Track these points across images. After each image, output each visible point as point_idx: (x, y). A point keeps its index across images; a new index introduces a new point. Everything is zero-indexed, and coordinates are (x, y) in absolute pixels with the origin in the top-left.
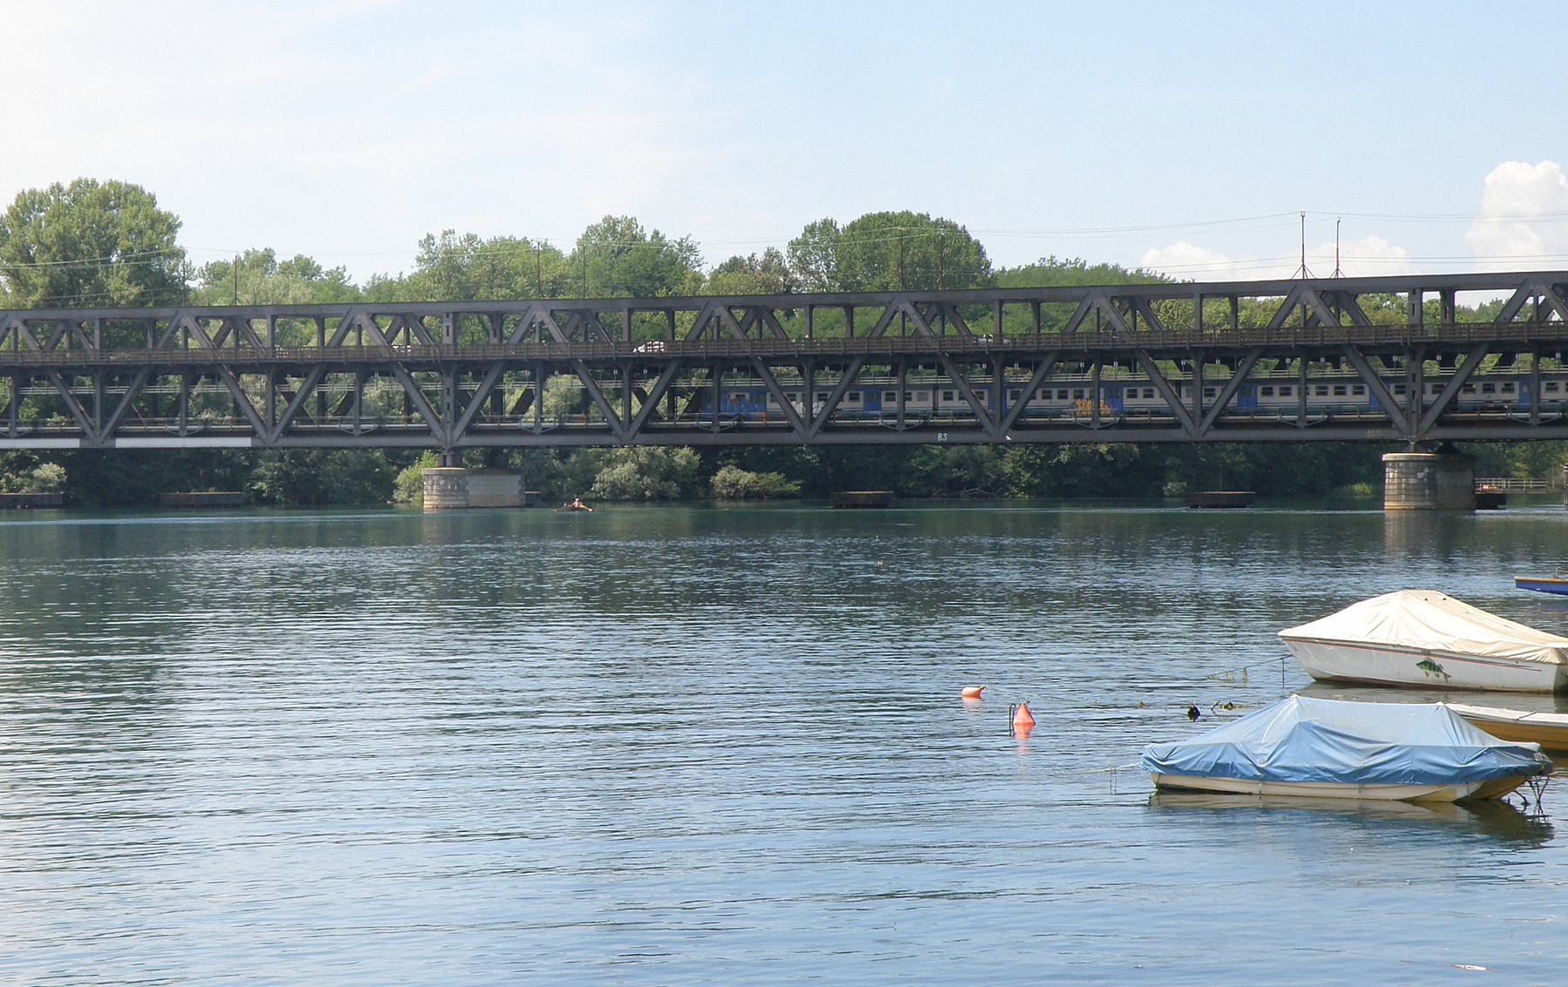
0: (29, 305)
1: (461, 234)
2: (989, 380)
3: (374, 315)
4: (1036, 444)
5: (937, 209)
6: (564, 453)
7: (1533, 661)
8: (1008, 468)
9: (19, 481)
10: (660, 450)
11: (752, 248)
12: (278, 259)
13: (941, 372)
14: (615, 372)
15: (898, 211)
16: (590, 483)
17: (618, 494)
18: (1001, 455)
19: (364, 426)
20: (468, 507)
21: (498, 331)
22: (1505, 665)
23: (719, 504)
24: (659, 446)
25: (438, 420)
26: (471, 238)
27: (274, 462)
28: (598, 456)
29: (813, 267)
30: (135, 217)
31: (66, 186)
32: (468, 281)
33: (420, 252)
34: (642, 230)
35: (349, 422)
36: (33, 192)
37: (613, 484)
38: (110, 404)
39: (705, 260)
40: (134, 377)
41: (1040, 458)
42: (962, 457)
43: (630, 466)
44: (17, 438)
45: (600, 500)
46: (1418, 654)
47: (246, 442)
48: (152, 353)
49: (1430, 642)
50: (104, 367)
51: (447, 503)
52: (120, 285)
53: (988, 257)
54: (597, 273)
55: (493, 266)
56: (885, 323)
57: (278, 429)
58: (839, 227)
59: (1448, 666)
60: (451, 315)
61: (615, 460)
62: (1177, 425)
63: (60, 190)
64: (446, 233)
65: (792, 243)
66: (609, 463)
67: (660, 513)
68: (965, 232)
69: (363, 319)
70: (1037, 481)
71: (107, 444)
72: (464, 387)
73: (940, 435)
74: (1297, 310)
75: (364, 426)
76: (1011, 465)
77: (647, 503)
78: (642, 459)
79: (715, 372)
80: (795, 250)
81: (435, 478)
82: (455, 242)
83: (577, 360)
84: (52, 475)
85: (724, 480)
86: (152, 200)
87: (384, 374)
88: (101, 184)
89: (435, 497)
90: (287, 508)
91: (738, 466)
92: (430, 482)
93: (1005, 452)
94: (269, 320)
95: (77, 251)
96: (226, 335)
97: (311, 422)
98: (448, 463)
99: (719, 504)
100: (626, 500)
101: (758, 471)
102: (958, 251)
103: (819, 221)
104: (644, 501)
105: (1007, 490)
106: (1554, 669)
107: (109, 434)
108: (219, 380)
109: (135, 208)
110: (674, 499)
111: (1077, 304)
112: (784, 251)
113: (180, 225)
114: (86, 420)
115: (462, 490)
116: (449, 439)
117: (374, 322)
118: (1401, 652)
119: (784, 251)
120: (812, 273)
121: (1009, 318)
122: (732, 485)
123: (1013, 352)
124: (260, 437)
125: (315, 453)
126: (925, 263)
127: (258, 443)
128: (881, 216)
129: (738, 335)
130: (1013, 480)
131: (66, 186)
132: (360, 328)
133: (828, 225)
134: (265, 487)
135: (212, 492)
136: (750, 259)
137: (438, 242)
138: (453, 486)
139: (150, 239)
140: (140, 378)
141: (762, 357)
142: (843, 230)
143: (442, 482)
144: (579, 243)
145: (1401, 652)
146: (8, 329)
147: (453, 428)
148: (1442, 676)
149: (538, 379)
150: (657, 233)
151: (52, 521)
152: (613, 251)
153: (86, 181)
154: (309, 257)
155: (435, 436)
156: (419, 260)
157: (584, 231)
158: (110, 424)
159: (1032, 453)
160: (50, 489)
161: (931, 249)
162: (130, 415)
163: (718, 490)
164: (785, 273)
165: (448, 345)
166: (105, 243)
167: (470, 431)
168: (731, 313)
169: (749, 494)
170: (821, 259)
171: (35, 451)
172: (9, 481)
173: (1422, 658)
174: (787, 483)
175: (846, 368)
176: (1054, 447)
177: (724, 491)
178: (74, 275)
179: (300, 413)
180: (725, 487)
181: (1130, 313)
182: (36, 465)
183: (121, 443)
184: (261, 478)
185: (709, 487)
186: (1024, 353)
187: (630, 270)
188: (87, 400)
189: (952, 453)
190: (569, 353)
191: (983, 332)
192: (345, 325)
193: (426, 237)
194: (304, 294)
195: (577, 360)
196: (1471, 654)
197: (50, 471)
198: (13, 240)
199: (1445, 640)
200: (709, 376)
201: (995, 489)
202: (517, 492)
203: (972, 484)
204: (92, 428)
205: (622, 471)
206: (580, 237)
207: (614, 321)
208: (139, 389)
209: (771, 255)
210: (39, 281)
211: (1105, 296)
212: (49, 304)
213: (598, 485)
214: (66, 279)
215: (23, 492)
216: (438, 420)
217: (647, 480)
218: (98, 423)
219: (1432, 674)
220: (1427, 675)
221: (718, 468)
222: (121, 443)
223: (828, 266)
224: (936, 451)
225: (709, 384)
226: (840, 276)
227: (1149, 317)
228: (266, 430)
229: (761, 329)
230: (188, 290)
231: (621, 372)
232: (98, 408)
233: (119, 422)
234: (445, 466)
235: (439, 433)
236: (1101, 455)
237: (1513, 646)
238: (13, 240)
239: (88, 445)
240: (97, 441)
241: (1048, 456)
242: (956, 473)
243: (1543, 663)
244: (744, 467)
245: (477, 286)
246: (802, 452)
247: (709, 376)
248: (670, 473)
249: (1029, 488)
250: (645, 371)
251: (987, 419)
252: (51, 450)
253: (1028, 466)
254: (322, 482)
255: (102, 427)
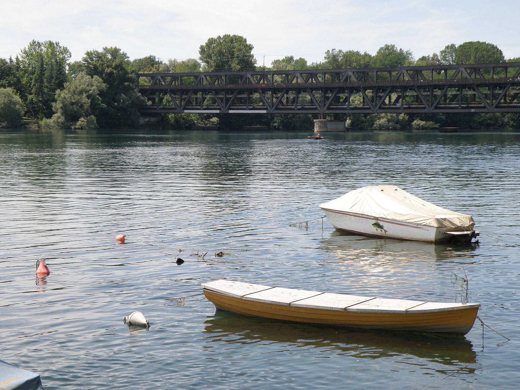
0: (210, 71)
1: (337, 50)
3: (301, 74)
4: (515, 113)
5: (489, 40)
8: (506, 120)
10: (394, 115)
12: (295, 59)
15: (475, 41)
16: (373, 124)
17: (381, 128)
18: (504, 116)
21: (338, 78)
22: (412, 227)
24: (394, 113)
27: (279, 117)
28: (376, 116)
29: (447, 59)
30: (240, 45)
31: (222, 37)
32: (339, 64)
33: (325, 55)
34: (396, 48)
36: (212, 39)
37: (380, 125)
38: (228, 100)
39: (414, 57)
41: (516, 117)
42: (491, 117)
43: (385, 119)
44: (203, 110)
45: (376, 129)
46: (373, 219)
47: (265, 112)
50: (226, 89)
51: (321, 130)
52: (235, 65)
53: (504, 55)
54: (381, 61)
55: (346, 59)
56: (455, 75)
58: (457, 46)
60: (324, 74)
61: (381, 118)
63: (220, 38)
64: (333, 50)
66: (379, 119)
67: (393, 134)
68: (497, 47)
69: (298, 75)
70: (515, 124)
71: (227, 112)
72: (327, 95)
73: (472, 110)
74: (460, 75)
76: (507, 119)
77: (390, 131)
78: (389, 117)
79: (460, 89)
80: (442, 54)
81: (318, 122)
82: (336, 53)
83: (360, 87)
86: (245, 41)
88: (231, 36)
89: (318, 128)
90: (283, 131)
91: (420, 119)
92: (316, 124)
95: (224, 56)
96: (261, 80)
97: (284, 106)
99: (414, 131)
100: (384, 130)
101: (426, 121)
102: (494, 53)
103: (450, 45)
104: (390, 130)
105: (506, 127)
106: (435, 230)
107: (227, 109)
108: (360, 91)
109: (240, 43)
110: (399, 129)
112: (439, 54)
113: (253, 48)
114: (221, 104)
115: (326, 126)
116: (322, 111)
117: (301, 76)
119: (439, 54)
120: (447, 61)
121: (509, 73)
122: (418, 125)
123: (497, 83)
124: (269, 110)
125: (290, 115)
126: (483, 56)
127: (268, 112)
128: (470, 43)
129: (468, 77)
130: (507, 124)
131: (222, 37)
132: (297, 77)
133: (453, 46)
135: (258, 126)
136: (428, 57)
138: (323, 125)
139: (244, 52)
140: (235, 93)
141: (476, 84)
142: (458, 47)
144: (378, 53)
146: (401, 74)
147: (323, 108)
148: (383, 231)
150: (401, 49)
152: (387, 55)
153: (227, 35)
154: (303, 58)
155: (318, 110)
157: (379, 49)
159: (514, 115)
161: (485, 53)
162: (233, 103)
163: (413, 127)
164: (439, 61)
165: (322, 83)
166: (232, 53)
167: (329, 108)
168: (301, 76)
169: (423, 128)
170: (450, 56)
171: (211, 114)
172: (204, 122)
173: (374, 222)
174: (435, 124)
175: (443, 89)
177: (415, 127)
178: (223, 62)
180: (416, 126)
182: (211, 118)
183: (231, 112)
184: (276, 122)
185: (411, 125)
186: (501, 84)
187: (391, 60)
188: (221, 99)
189: (488, 116)
190: (358, 85)
192: (293, 77)
194: (291, 68)
195: (360, 87)
196: (396, 220)
197: (215, 119)
198: (206, 53)
200: (458, 91)
201: (502, 127)
202: (343, 127)
203: (494, 125)
204: (223, 107)
206: (378, 51)
207: (383, 76)
208: (235, 96)
209: (435, 55)
212: (216, 71)
213: (375, 125)
216: (319, 105)
217: (390, 124)
218: (224, 105)
219: (379, 230)
220: (377, 230)
221: (414, 120)
222: (231, 112)
223: (452, 58)
225: (458, 93)
228: (270, 108)
230: (255, 67)
231: (429, 89)
233: (230, 106)
234: (321, 119)
235: (320, 109)
238: (206, 53)
240: (224, 111)
242: (489, 122)
243: (429, 226)
244: (422, 120)
246: (440, 115)
247: (458, 91)
248: (398, 122)
249: (513, 126)
250: (381, 90)
251: (488, 105)
252: (215, 113)
253: (512, 120)
254: (292, 124)
255: (226, 107)
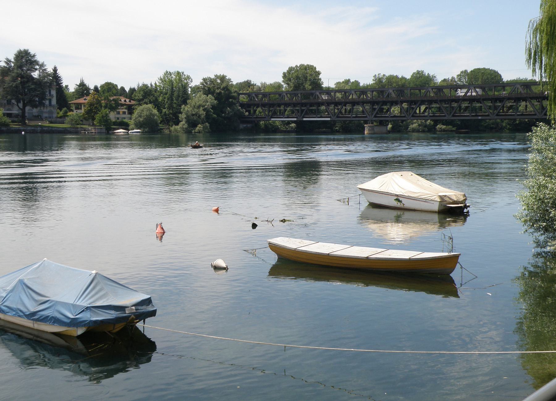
1: (382, 74)
2: (448, 106)
3: (356, 92)
5: (492, 67)
6: (403, 121)
7: (431, 200)
8: (504, 124)
9: (287, 127)
11: (449, 76)
12: (351, 81)
13: (481, 103)
14: (447, 103)
15: (482, 68)
17: (414, 130)
18: (503, 122)
19: (353, 116)
20: (374, 133)
22: (422, 201)
23: (438, 133)
24: (423, 120)
25: (368, 114)
26: (384, 75)
28: (410, 122)
29: (462, 80)
31: (298, 66)
33: (373, 78)
35: (315, 115)
36: (292, 67)
37: (413, 128)
38: (302, 111)
40: (417, 103)
43: (417, 124)
47: (329, 119)
48: (312, 100)
49: (398, 191)
52: (308, 86)
53: (503, 77)
54: (413, 82)
57: (336, 116)
58: (469, 71)
59: (404, 201)
61: (413, 123)
62: (535, 115)
63: (297, 66)
65: (457, 75)
66: (412, 124)
69: (353, 92)
70: (511, 128)
71: (302, 119)
75: (353, 116)
76: (505, 124)
78: (419, 123)
82: (381, 76)
84: (293, 126)
85: (439, 127)
86: (315, 68)
87: (435, 103)
91: (442, 124)
93: (504, 121)
94: (334, 93)
95: (300, 79)
98: (370, 123)
101: (446, 125)
102: (495, 76)
103: (464, 70)
106: (438, 203)
109: (311, 70)
110: (426, 132)
111: (513, 87)
112: (456, 77)
115: (373, 129)
117: (356, 93)
118: (389, 195)
119: (456, 77)
120: (462, 82)
122: (441, 128)
130: (505, 127)
131: (298, 66)
132: (353, 94)
133: (466, 71)
134: (338, 129)
137: (377, 76)
143: (369, 128)
144: (411, 76)
145: (389, 195)
148: (402, 204)
149: (471, 104)
150: (428, 74)
151: (293, 136)
155: (368, 118)
156: (373, 80)
158: (302, 116)
159: (510, 121)
160: (293, 129)
162: (307, 113)
164: (456, 82)
167: (375, 117)
168: (356, 93)
169: (444, 130)
170: (464, 79)
171: (291, 121)
173: (396, 198)
176: (515, 120)
177: (439, 130)
178: (299, 84)
179: (341, 112)
180: (439, 129)
181: (526, 89)
182: (291, 124)
183: (305, 119)
184: (337, 127)
185: (435, 129)
187: (421, 82)
188: (298, 110)
189: (491, 121)
191: (504, 93)
193: (374, 75)
194: (348, 88)
196: (411, 197)
197: (293, 125)
199: (403, 191)
200: (469, 104)
204: (299, 116)
205: (415, 125)
209: (453, 78)
210: (292, 86)
211: (519, 85)
213: (409, 128)
214: (297, 85)
215: (288, 129)
217: (420, 127)
219: (399, 203)
220: (398, 204)
221: (437, 125)
222: (305, 119)
224: (487, 121)
225: (469, 105)
226: (468, 82)
227: (530, 90)
229: (527, 90)
231: (448, 102)
232: (300, 112)
233: (304, 115)
236: (526, 122)
237: (425, 194)
239: (298, 120)
240: (300, 119)
241: (514, 122)
242: (492, 126)
243: (434, 201)
244: (444, 125)
245: (385, 85)
247: (469, 104)
248: (426, 126)
249: (509, 129)
253: (509, 124)
